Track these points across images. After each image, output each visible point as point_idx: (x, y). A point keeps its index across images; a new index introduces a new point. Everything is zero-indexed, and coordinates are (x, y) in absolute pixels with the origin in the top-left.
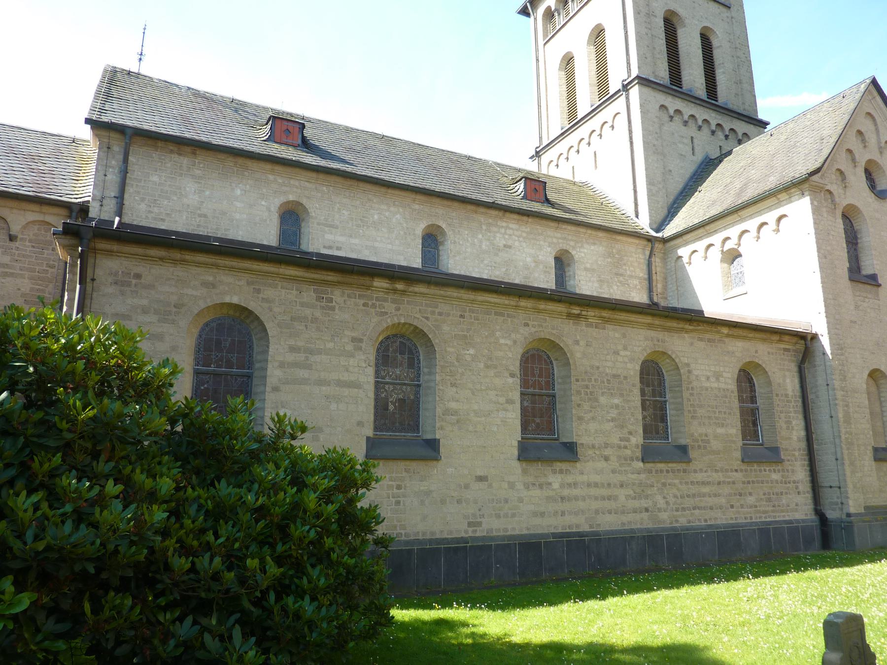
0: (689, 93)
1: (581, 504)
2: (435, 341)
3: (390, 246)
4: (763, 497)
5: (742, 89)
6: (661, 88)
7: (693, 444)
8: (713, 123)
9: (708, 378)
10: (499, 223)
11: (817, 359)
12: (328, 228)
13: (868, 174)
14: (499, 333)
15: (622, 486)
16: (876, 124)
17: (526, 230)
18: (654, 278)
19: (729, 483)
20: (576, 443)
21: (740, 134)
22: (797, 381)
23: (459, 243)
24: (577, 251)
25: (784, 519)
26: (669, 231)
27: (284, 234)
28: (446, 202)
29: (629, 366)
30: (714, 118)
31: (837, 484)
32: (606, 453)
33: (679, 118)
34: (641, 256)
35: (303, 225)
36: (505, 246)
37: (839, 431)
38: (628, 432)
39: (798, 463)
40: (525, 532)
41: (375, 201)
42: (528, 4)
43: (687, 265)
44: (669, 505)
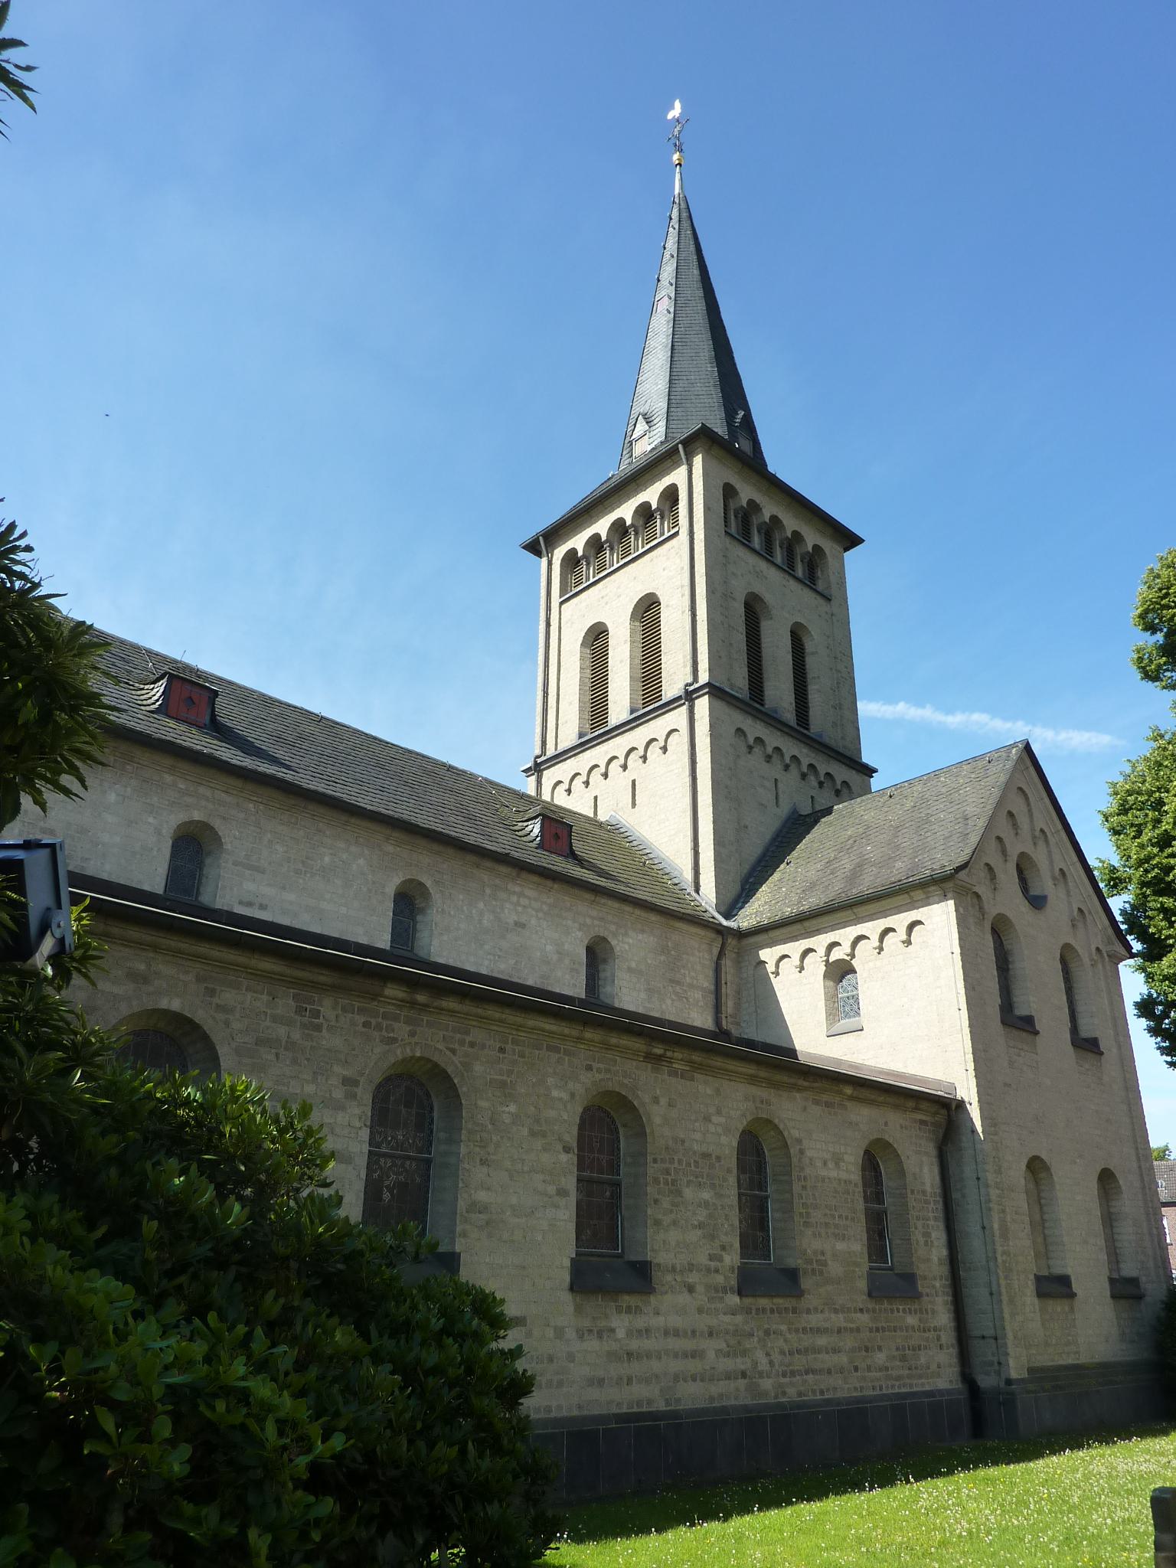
0: (818, 738)
1: (656, 1366)
2: (463, 1090)
3: (344, 910)
4: (896, 1353)
5: (841, 716)
6: (738, 704)
7: (805, 1266)
8: (822, 772)
9: (825, 1163)
10: (510, 886)
11: (964, 1139)
12: (249, 872)
13: (1020, 870)
14: (552, 1079)
15: (711, 1334)
16: (1029, 805)
17: (549, 901)
18: (723, 990)
19: (851, 1330)
20: (651, 1262)
21: (839, 783)
22: (936, 1170)
23: (449, 913)
24: (619, 941)
25: (924, 1389)
26: (747, 918)
27: (175, 874)
28: (435, 847)
29: (724, 1140)
30: (806, 756)
31: (992, 1332)
32: (690, 1280)
33: (760, 750)
34: (706, 956)
35: (208, 861)
36: (516, 923)
37: (995, 1249)
38: (720, 1246)
39: (940, 1300)
40: (575, 1413)
41: (328, 833)
42: (541, 538)
43: (772, 976)
44: (774, 1366)
